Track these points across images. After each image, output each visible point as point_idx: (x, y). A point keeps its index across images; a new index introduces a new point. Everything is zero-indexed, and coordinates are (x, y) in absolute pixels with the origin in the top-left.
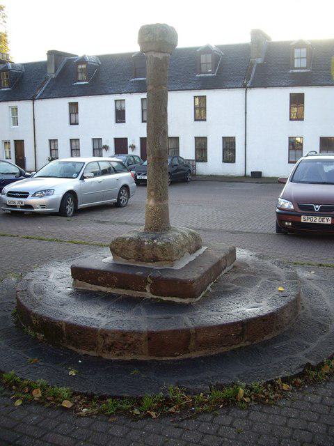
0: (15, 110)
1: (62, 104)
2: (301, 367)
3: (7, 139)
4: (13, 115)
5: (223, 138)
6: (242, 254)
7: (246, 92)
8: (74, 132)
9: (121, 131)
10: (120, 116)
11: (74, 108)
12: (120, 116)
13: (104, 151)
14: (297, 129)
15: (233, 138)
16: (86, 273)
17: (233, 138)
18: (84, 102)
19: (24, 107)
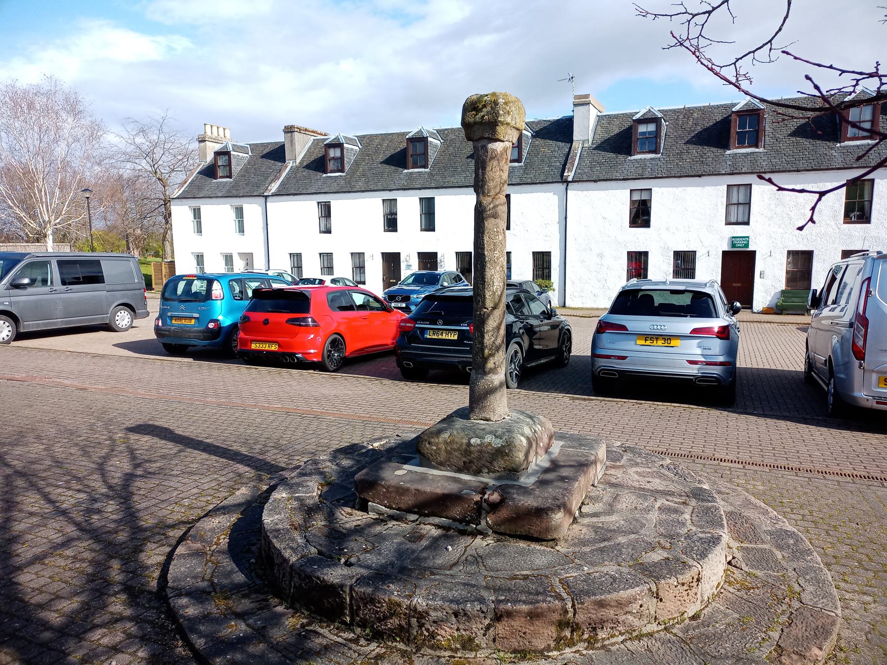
0: (239, 212)
1: (308, 207)
2: (431, 579)
3: (228, 251)
4: (198, 265)
5: (533, 252)
6: (473, 441)
7: (567, 189)
8: (326, 244)
9: (391, 243)
10: (391, 224)
11: (326, 211)
12: (391, 224)
13: (5, 506)
14: (639, 239)
15: (548, 254)
16: (741, 410)
17: (548, 254)
18: (340, 205)
19: (252, 209)
